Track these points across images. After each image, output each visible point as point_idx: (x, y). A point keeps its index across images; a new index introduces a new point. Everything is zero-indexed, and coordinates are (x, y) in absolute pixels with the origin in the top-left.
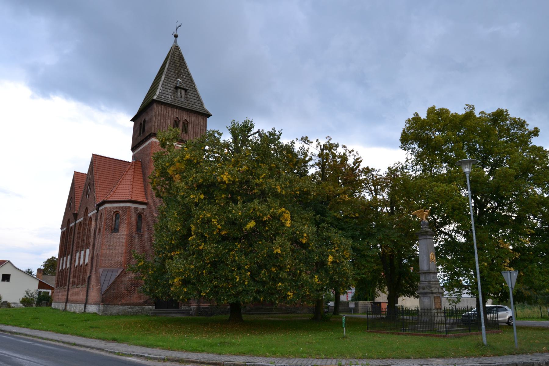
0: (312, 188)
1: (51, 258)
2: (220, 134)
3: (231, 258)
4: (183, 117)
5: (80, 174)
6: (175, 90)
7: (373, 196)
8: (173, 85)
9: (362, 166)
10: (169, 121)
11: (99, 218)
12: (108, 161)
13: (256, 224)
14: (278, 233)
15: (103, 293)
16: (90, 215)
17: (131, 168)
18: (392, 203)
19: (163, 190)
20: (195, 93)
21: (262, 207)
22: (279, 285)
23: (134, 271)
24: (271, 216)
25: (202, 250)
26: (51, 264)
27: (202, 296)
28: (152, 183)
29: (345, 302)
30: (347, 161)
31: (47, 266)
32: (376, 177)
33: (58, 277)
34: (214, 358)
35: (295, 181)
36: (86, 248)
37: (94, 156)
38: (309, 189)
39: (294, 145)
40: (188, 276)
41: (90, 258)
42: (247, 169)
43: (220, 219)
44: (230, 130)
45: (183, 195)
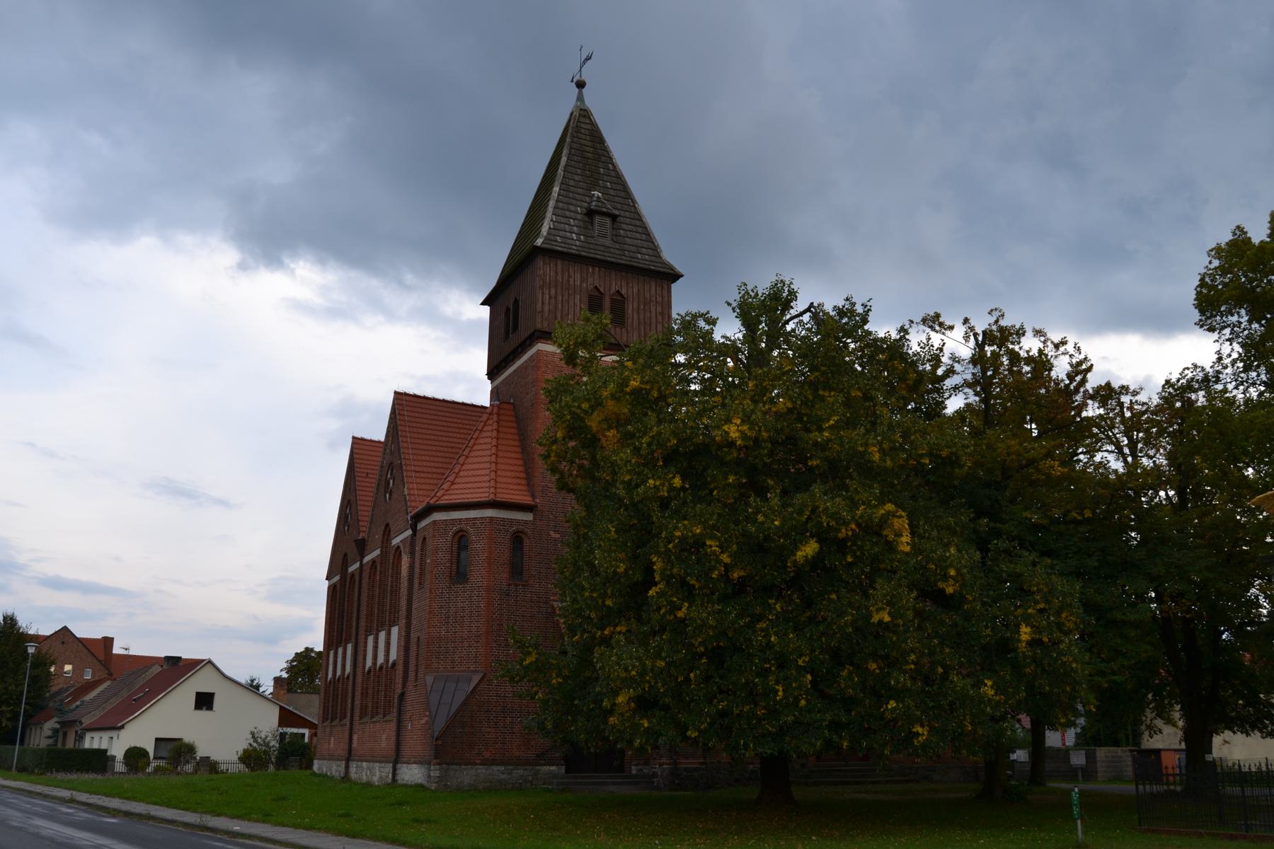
0: (963, 446)
2: (712, 322)
4: (613, 284)
5: (368, 443)
6: (586, 219)
7: (1125, 461)
8: (581, 207)
9: (1093, 381)
12: (431, 407)
13: (821, 548)
15: (436, 734)
16: (396, 541)
17: (491, 422)
18: (1182, 473)
19: (575, 472)
20: (638, 223)
21: (834, 504)
22: (889, 707)
24: (858, 525)
26: (304, 664)
27: (689, 738)
28: (546, 457)
29: (1059, 750)
30: (1050, 370)
32: (1131, 408)
37: (400, 398)
38: (954, 450)
39: (907, 337)
40: (650, 687)
42: (789, 405)
43: (726, 539)
44: (738, 311)
45: (630, 480)
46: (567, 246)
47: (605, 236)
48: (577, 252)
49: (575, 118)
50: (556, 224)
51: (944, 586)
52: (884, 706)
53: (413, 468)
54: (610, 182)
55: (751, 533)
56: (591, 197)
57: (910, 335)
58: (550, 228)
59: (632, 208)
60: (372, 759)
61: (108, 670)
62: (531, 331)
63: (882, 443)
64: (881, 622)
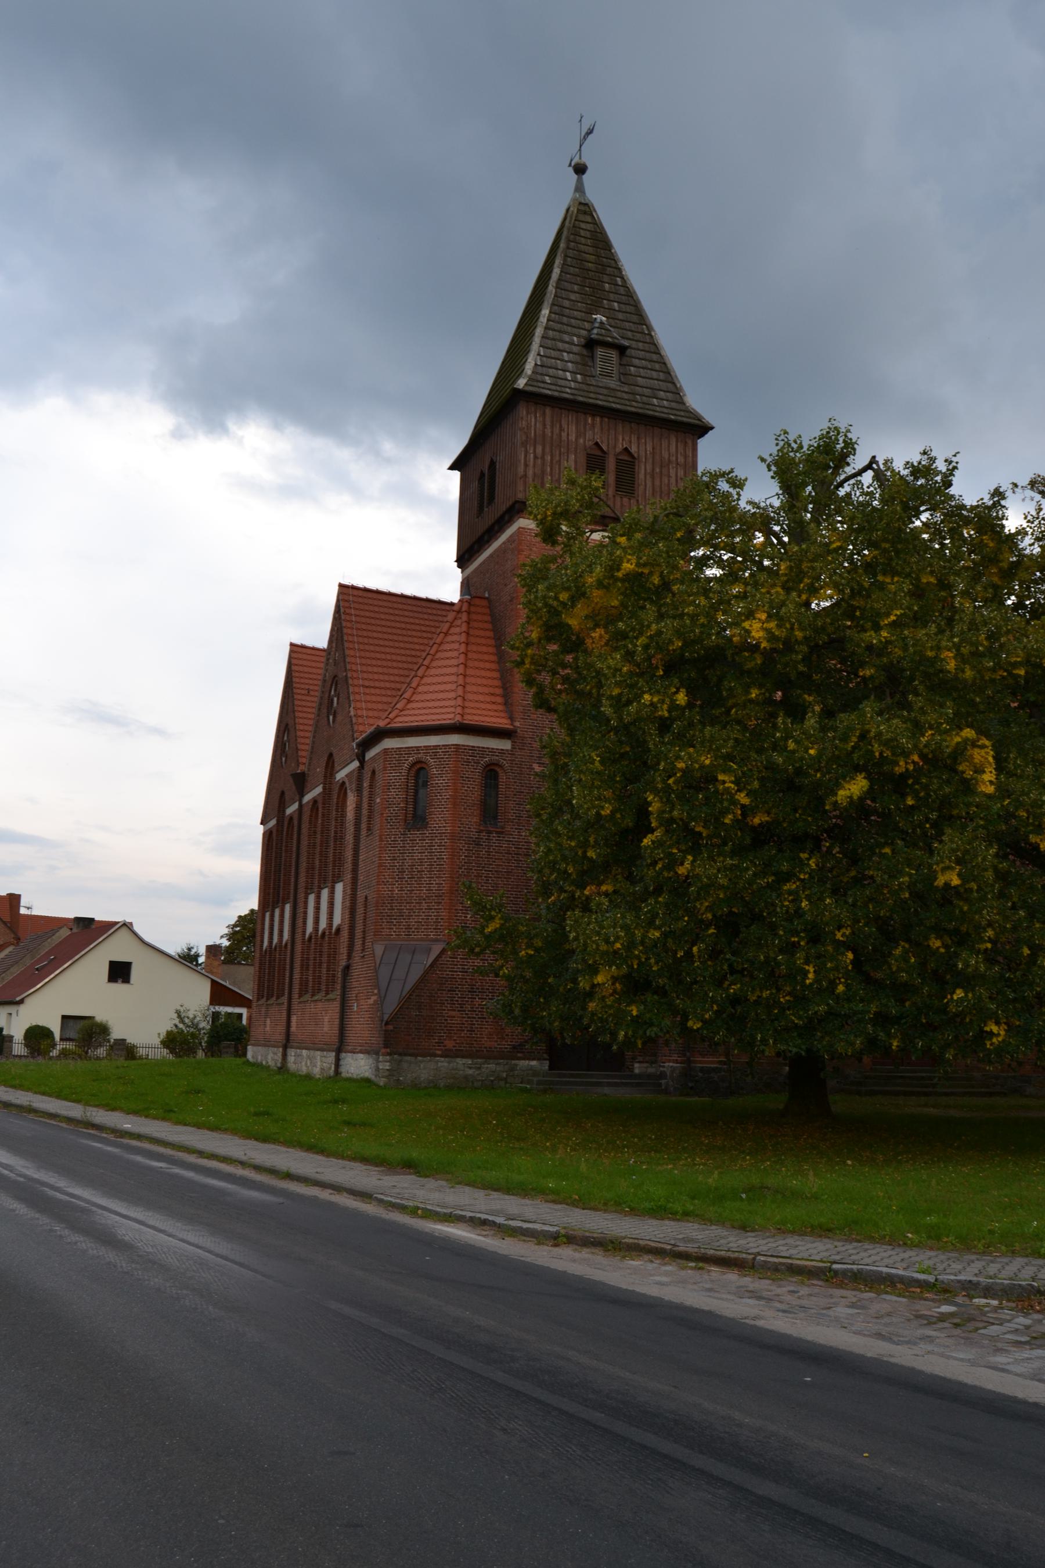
1: (247, 912)
2: (738, 484)
3: (787, 903)
5: (309, 652)
6: (585, 352)
8: (578, 336)
10: (572, 457)
11: (365, 785)
13: (871, 788)
14: (951, 817)
15: (386, 1017)
16: (340, 775)
17: (458, 622)
20: (655, 357)
21: (890, 727)
23: (472, 950)
24: (923, 756)
25: (687, 877)
27: (691, 1030)
31: (239, 936)
33: (260, 968)
34: (722, 1241)
35: (1008, 632)
36: (336, 879)
37: (345, 591)
39: (1003, 502)
41: (347, 911)
43: (743, 773)
44: (773, 468)
45: (620, 694)
46: (558, 388)
47: (609, 375)
48: (571, 397)
49: (572, 214)
50: (545, 359)
51: (1038, 840)
52: (949, 997)
53: (361, 682)
54: (618, 302)
55: (778, 765)
56: (592, 323)
57: (1008, 500)
58: (536, 364)
59: (647, 337)
60: (314, 1046)
61: (14, 932)
62: (511, 503)
63: (960, 646)
64: (947, 885)
